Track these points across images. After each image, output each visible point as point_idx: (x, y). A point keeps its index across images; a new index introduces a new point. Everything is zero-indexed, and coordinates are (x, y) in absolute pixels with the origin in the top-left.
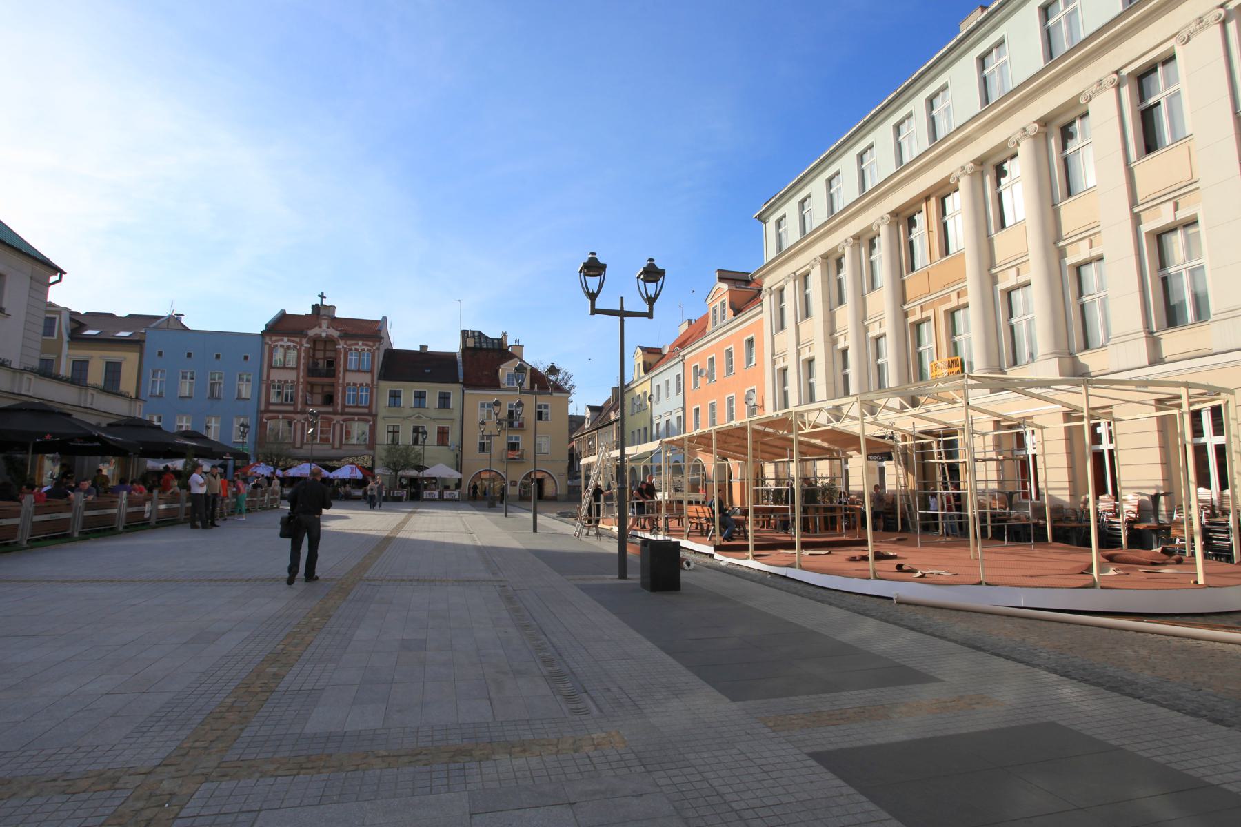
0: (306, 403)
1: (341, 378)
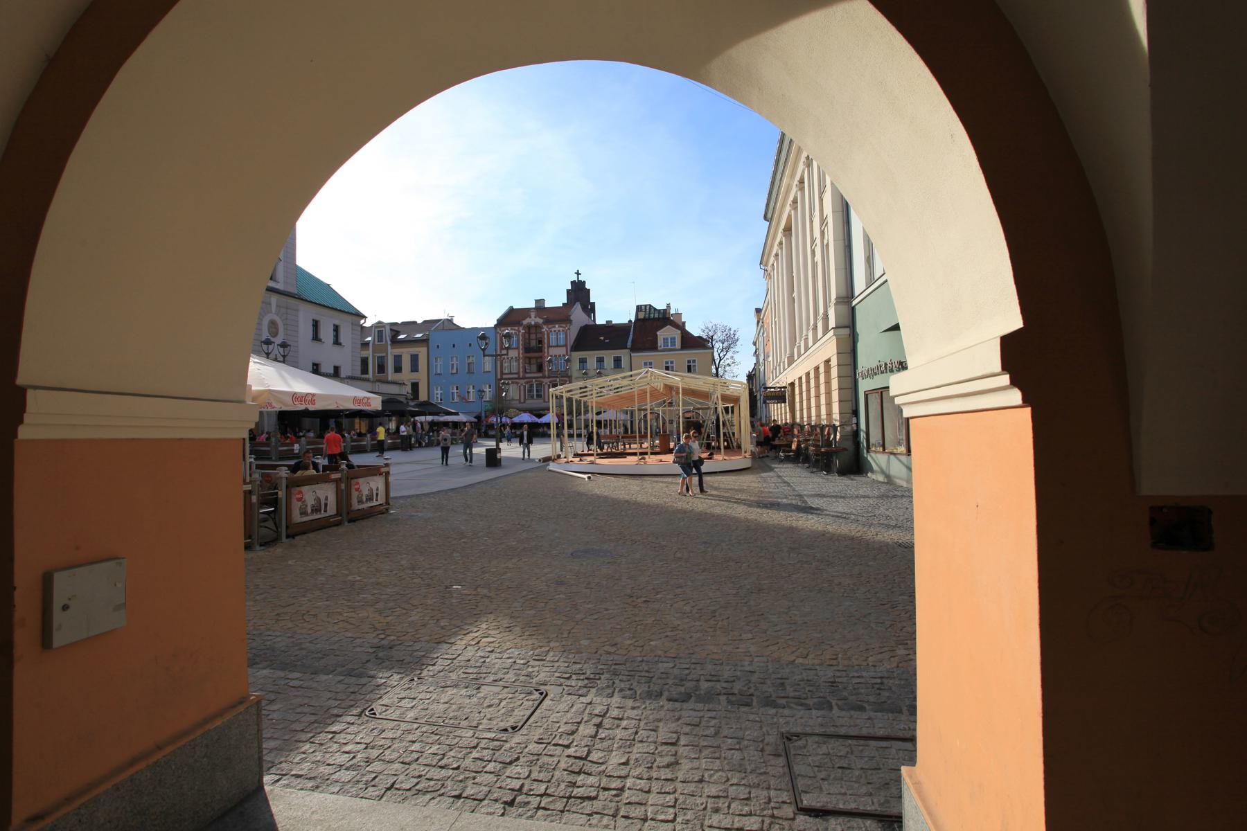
0: (526, 372)
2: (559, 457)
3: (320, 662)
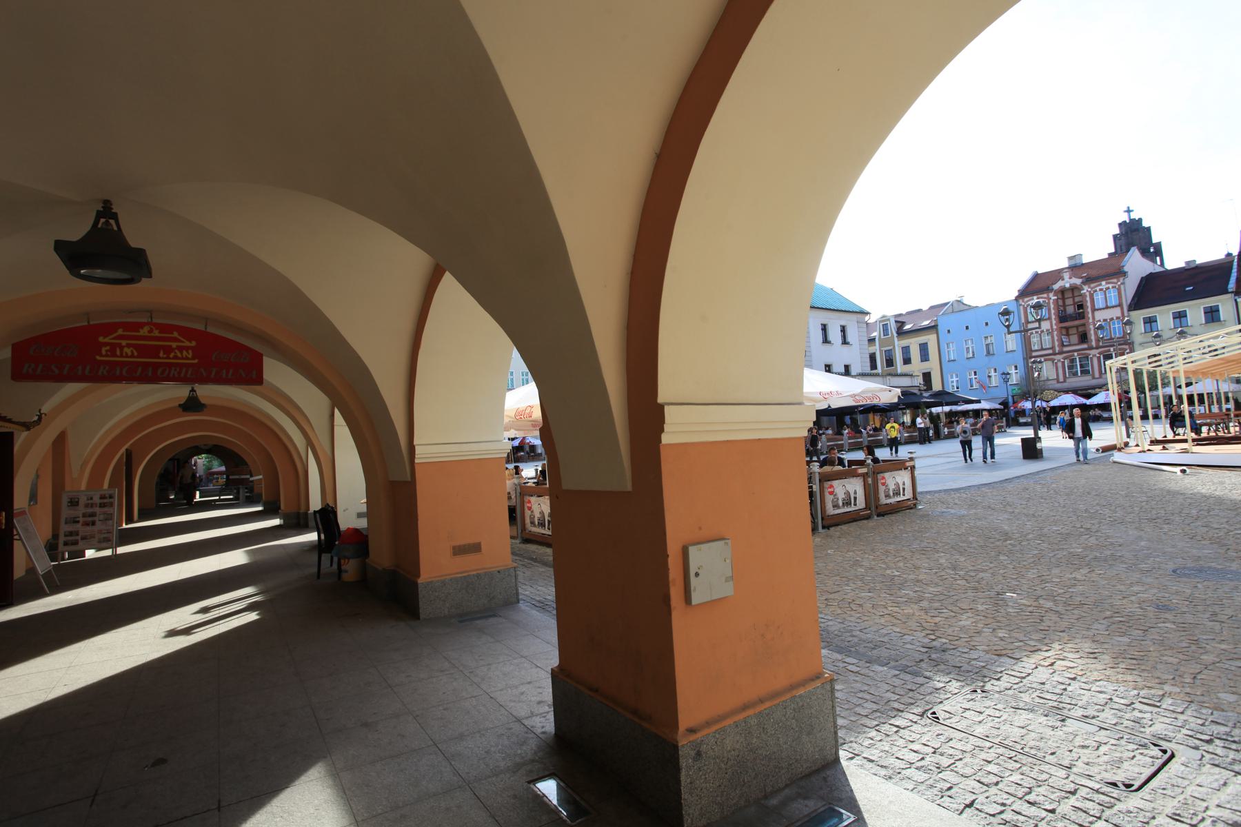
0: (1062, 345)
1: (1091, 318)
2: (1126, 444)
3: (873, 652)
